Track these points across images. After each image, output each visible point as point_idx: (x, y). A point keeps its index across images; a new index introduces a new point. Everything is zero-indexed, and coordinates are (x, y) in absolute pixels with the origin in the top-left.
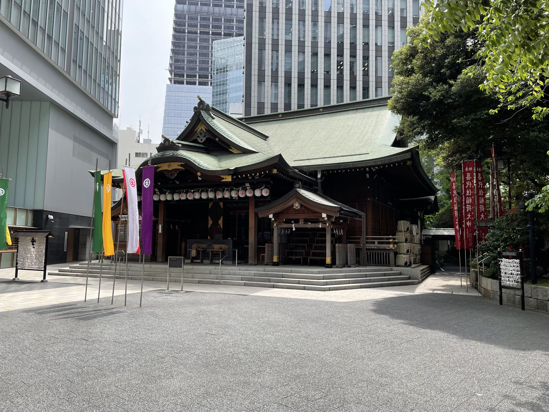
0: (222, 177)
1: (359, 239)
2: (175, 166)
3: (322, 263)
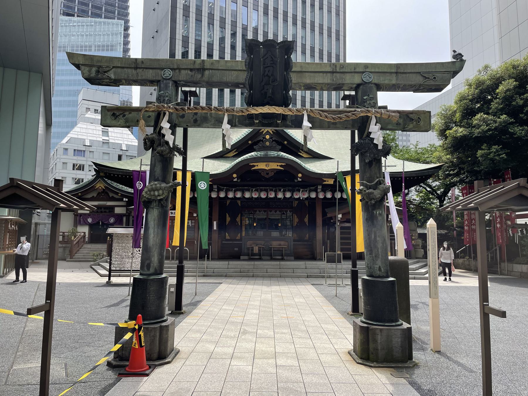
0: (324, 179)
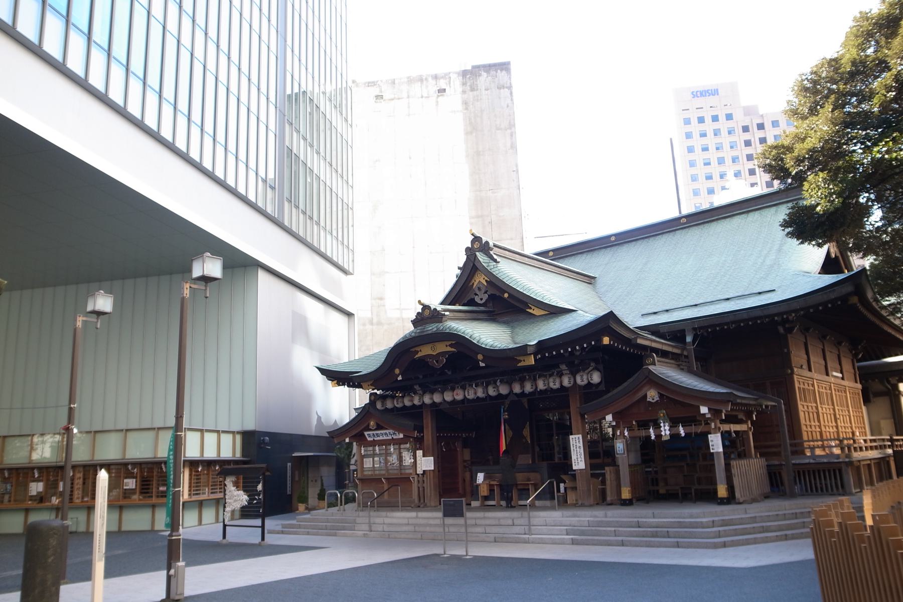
1: (780, 446)
2: (442, 347)
3: (708, 496)
